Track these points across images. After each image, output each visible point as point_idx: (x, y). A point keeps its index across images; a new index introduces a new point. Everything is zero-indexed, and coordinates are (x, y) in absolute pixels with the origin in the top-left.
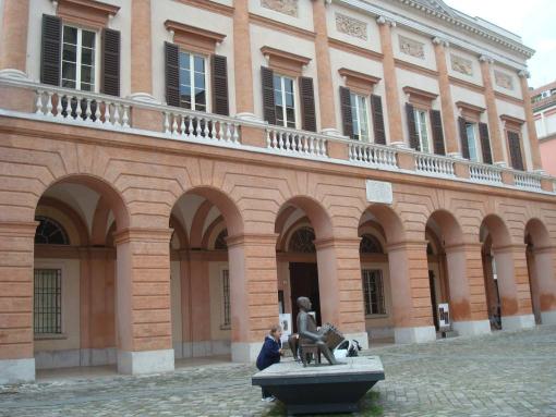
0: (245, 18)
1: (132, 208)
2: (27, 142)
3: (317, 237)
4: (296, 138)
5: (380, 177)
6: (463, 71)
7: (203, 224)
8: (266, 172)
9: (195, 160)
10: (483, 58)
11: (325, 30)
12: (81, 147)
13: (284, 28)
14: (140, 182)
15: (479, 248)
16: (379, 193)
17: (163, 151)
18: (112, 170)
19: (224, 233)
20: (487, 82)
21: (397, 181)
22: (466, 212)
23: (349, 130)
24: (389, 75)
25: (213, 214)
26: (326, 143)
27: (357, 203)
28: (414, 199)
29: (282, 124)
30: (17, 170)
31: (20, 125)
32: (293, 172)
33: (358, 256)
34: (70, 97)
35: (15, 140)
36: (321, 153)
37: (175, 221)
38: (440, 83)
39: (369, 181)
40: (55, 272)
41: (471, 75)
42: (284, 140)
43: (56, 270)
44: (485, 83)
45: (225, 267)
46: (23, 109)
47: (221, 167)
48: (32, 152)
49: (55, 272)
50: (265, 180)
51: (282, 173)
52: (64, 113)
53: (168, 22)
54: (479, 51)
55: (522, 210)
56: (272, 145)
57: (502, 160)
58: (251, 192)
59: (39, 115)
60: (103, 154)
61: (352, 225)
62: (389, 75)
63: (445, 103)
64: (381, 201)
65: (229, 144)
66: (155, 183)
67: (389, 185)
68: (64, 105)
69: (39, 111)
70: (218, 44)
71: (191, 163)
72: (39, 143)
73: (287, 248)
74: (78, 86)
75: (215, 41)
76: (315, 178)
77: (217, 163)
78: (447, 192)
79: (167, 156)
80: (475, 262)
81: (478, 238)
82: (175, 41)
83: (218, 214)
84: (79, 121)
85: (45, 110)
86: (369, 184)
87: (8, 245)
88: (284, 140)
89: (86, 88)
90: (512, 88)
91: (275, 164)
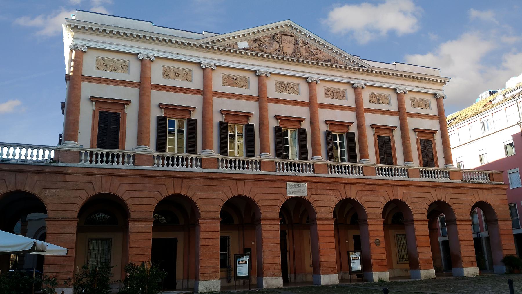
1: (262, 209)
2: (75, 178)
4: (385, 169)
5: (297, 180)
6: (379, 102)
8: (216, 183)
9: (171, 180)
10: (203, 66)
12: (104, 179)
14: (137, 194)
15: (76, 223)
17: (264, 180)
18: (122, 190)
21: (309, 181)
22: (371, 199)
23: (223, 150)
24: (262, 109)
27: (280, 197)
29: (336, 160)
30: (69, 193)
31: (70, 170)
32: (234, 182)
33: (383, 229)
35: (68, 178)
38: (140, 91)
39: (290, 183)
40: (109, 240)
42: (391, 171)
43: (109, 239)
44: (399, 108)
45: (357, 233)
46: (74, 161)
47: (187, 182)
48: (77, 183)
49: (109, 240)
50: (214, 187)
51: (226, 183)
52: (102, 162)
53: (160, 105)
54: (136, 51)
55: (428, 195)
56: (331, 172)
57: (320, 155)
58: (205, 195)
60: (116, 181)
63: (360, 126)
64: (298, 195)
66: (146, 194)
67: (305, 184)
71: (169, 182)
72: (81, 178)
74: (176, 151)
76: (249, 184)
77: (399, 188)
79: (154, 179)
82: (280, 124)
84: (104, 165)
85: (158, 165)
86: (289, 184)
87: (62, 231)
89: (343, 160)
90: (429, 108)
91: (222, 178)
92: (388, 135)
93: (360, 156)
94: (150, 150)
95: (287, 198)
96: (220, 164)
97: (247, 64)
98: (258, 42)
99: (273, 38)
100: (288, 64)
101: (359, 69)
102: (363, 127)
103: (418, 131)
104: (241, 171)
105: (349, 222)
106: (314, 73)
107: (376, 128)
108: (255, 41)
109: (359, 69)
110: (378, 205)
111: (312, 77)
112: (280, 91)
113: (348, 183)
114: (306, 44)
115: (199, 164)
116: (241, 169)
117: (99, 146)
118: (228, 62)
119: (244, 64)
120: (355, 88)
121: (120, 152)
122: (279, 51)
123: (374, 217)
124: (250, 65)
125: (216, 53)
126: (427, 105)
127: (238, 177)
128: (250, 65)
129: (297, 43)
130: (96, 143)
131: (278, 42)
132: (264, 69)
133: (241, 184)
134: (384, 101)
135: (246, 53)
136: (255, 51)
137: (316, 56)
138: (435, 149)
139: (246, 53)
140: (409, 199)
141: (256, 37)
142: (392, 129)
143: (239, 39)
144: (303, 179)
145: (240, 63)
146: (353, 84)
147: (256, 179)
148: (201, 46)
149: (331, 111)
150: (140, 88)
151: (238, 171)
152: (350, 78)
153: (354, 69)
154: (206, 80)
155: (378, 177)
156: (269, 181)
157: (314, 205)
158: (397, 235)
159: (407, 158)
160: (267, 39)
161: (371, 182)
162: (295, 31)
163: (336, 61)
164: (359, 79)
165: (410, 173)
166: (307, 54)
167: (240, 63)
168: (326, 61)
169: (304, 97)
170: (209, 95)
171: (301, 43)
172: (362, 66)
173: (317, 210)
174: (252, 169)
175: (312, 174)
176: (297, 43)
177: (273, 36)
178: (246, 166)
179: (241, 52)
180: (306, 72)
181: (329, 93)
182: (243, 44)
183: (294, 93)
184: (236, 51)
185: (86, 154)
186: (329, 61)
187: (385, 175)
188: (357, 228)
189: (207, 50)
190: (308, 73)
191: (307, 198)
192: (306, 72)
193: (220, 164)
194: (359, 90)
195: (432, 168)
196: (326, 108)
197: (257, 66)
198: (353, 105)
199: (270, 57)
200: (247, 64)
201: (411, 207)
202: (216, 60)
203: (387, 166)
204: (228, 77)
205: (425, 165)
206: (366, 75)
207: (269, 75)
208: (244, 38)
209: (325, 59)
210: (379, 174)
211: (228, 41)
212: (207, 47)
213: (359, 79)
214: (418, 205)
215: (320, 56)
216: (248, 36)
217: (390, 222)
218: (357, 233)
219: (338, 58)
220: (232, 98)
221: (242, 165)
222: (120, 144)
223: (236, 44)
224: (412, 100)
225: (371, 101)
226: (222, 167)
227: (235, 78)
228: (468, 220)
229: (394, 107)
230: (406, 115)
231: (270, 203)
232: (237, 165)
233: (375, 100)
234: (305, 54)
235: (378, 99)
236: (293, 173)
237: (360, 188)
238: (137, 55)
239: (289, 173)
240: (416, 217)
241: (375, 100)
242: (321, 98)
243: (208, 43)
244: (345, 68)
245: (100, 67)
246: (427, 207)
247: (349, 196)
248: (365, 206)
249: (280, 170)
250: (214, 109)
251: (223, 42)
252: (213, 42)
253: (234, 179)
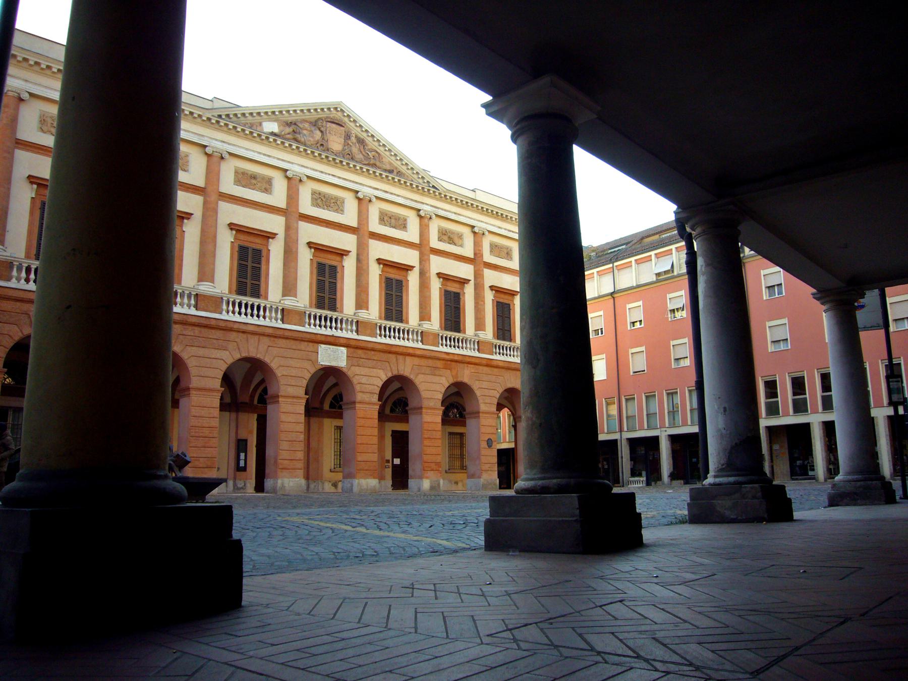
0: (367, 234)
3: (344, 398)
4: (246, 305)
6: (451, 241)
7: (251, 382)
10: (289, 174)
11: (297, 205)
13: (42, 150)
16: (332, 357)
19: (265, 391)
20: (478, 253)
21: (347, 344)
24: (478, 275)
25: (331, 381)
26: (283, 310)
28: (370, 363)
32: (245, 336)
34: (262, 305)
36: (352, 331)
37: (227, 379)
39: (323, 346)
41: (461, 246)
42: (320, 320)
44: (475, 254)
51: (233, 335)
53: (30, 177)
58: (201, 352)
59: (13, 284)
61: (300, 384)
62: (478, 275)
65: (274, 324)
67: (344, 350)
68: (252, 309)
69: (14, 280)
70: (185, 221)
73: (256, 402)
75: (342, 255)
76: (266, 341)
78: (408, 359)
80: (212, 410)
81: (376, 397)
83: (335, 381)
86: (322, 348)
88: (320, 320)
91: (227, 328)
92: (458, 291)
93: (823, 387)
94: (5, 254)
95: (319, 367)
96: (225, 307)
97: (274, 158)
98: (293, 127)
99: (315, 124)
100: (332, 166)
101: (429, 190)
102: (427, 275)
103: (497, 290)
104: (249, 320)
105: (326, 407)
106: (368, 186)
107: (315, 249)
108: (289, 124)
109: (429, 190)
110: (438, 387)
111: (365, 191)
112: (318, 206)
113: (254, 333)
114: (361, 141)
115: (193, 302)
116: (243, 315)
117: (446, 329)
118: (247, 149)
119: (269, 156)
120: (359, 199)
121: (334, 315)
122: (322, 145)
123: (432, 404)
124: (279, 159)
125: (230, 134)
126: (401, 224)
127: (251, 328)
128: (279, 159)
129: (348, 136)
130: (234, 287)
131: (322, 132)
132: (297, 169)
133: (253, 340)
134: (456, 240)
135: (275, 140)
136: (288, 139)
137: (372, 162)
138: (440, 299)
139: (275, 140)
140: (477, 382)
141: (290, 119)
142: (463, 282)
143: (265, 117)
144: (342, 341)
145: (264, 155)
146: (419, 210)
147: (275, 335)
148: (209, 119)
149: (386, 245)
150: (358, 235)
151: (249, 320)
152: (283, 160)
153: (423, 188)
154: (292, 196)
155: (441, 349)
156: (295, 339)
157: (355, 381)
158: (450, 434)
159: (362, 303)
160: (307, 125)
161: (433, 354)
162: (346, 119)
163: (399, 173)
164: (428, 205)
165: (200, 304)
166: (361, 156)
167: (264, 155)
168: (386, 171)
169: (350, 217)
170: (213, 197)
171: (353, 139)
172: (433, 187)
173: (358, 388)
174: (271, 318)
175: (354, 336)
176: (348, 136)
177: (316, 121)
178: (262, 313)
179: (267, 138)
180: (357, 183)
181: (386, 218)
182: (271, 127)
183: (336, 211)
184: (259, 136)
185: (19, 269)
186: (391, 172)
187: (320, 326)
188: (340, 416)
189: (217, 126)
190: (361, 184)
191: (345, 370)
192: (357, 183)
193: (225, 307)
194: (426, 220)
195: (508, 343)
196: (379, 240)
197: (289, 162)
198: (416, 240)
199: (255, 135)
200: (274, 158)
201: (478, 393)
202: (229, 144)
203: (393, 324)
204: (243, 173)
205: (388, 317)
206: (437, 200)
207: (226, 156)
208: (273, 116)
209: (385, 167)
210: (380, 335)
211: (250, 118)
212: (218, 122)
213: (428, 205)
214: (486, 392)
215: (378, 164)
216: (280, 116)
217: (387, 411)
218: (338, 422)
219: (403, 169)
220: (247, 207)
221: (255, 312)
222: (338, 305)
223: (260, 124)
224: (236, 172)
225: (440, 240)
226: (19, 279)
227: (254, 177)
228: (493, 413)
229: (468, 252)
230: (482, 266)
231: (294, 372)
232: (249, 310)
233: (445, 238)
234: (359, 156)
235: (449, 237)
236: (328, 332)
237: (416, 361)
238: (205, 147)
239: (323, 331)
240: (359, 397)
241: (445, 238)
242: (228, 185)
243: (220, 116)
244: (411, 185)
245: (45, 128)
246: (443, 390)
247: (401, 373)
248: (421, 387)
249: (228, 312)
250: (219, 221)
251: (242, 118)
252: (228, 116)
253: (244, 332)
